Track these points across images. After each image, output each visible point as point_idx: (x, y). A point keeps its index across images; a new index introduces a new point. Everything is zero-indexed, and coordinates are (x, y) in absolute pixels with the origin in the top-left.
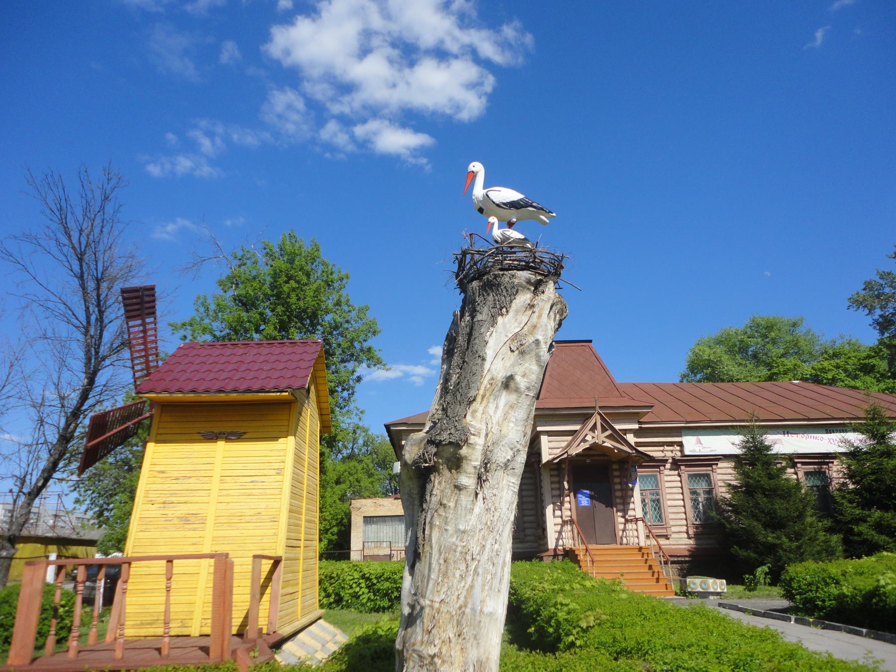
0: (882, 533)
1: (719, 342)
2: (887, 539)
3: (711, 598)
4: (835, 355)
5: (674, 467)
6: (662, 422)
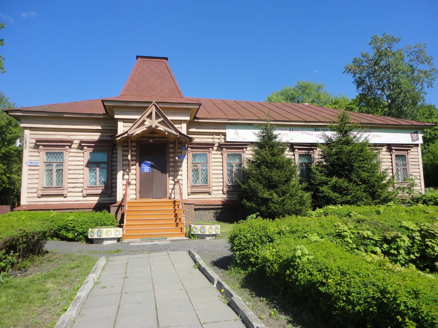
0: (336, 192)
1: (282, 94)
2: (338, 195)
3: (208, 238)
4: (336, 103)
5: (220, 149)
6: (212, 119)
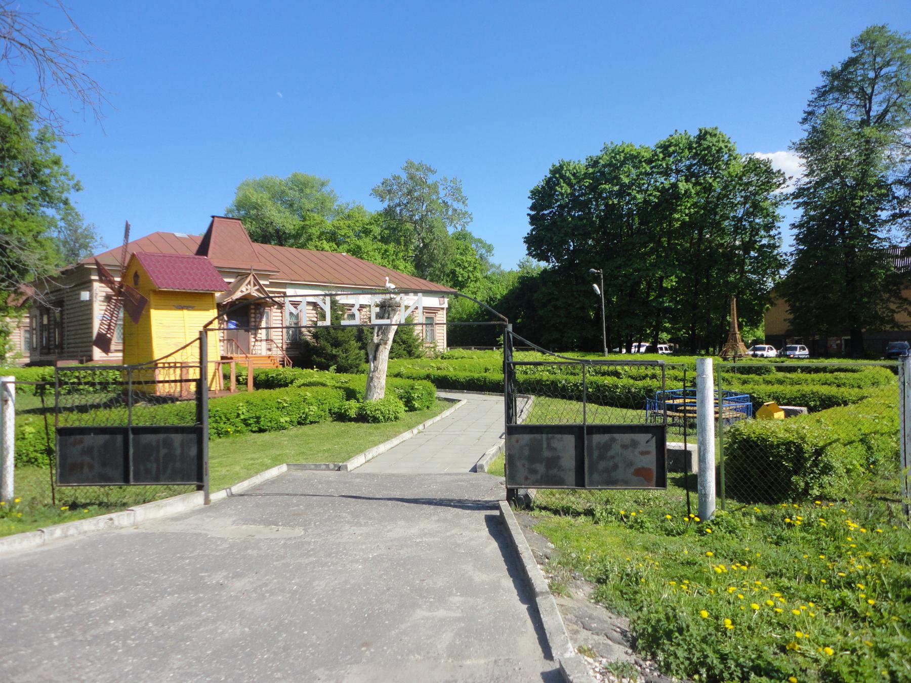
4: (349, 217)
